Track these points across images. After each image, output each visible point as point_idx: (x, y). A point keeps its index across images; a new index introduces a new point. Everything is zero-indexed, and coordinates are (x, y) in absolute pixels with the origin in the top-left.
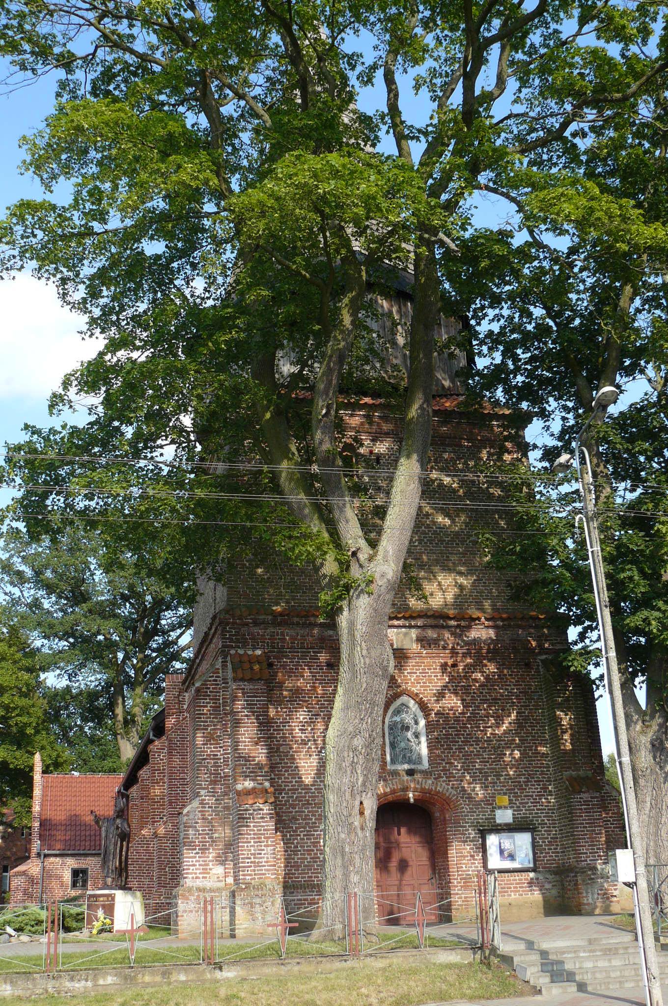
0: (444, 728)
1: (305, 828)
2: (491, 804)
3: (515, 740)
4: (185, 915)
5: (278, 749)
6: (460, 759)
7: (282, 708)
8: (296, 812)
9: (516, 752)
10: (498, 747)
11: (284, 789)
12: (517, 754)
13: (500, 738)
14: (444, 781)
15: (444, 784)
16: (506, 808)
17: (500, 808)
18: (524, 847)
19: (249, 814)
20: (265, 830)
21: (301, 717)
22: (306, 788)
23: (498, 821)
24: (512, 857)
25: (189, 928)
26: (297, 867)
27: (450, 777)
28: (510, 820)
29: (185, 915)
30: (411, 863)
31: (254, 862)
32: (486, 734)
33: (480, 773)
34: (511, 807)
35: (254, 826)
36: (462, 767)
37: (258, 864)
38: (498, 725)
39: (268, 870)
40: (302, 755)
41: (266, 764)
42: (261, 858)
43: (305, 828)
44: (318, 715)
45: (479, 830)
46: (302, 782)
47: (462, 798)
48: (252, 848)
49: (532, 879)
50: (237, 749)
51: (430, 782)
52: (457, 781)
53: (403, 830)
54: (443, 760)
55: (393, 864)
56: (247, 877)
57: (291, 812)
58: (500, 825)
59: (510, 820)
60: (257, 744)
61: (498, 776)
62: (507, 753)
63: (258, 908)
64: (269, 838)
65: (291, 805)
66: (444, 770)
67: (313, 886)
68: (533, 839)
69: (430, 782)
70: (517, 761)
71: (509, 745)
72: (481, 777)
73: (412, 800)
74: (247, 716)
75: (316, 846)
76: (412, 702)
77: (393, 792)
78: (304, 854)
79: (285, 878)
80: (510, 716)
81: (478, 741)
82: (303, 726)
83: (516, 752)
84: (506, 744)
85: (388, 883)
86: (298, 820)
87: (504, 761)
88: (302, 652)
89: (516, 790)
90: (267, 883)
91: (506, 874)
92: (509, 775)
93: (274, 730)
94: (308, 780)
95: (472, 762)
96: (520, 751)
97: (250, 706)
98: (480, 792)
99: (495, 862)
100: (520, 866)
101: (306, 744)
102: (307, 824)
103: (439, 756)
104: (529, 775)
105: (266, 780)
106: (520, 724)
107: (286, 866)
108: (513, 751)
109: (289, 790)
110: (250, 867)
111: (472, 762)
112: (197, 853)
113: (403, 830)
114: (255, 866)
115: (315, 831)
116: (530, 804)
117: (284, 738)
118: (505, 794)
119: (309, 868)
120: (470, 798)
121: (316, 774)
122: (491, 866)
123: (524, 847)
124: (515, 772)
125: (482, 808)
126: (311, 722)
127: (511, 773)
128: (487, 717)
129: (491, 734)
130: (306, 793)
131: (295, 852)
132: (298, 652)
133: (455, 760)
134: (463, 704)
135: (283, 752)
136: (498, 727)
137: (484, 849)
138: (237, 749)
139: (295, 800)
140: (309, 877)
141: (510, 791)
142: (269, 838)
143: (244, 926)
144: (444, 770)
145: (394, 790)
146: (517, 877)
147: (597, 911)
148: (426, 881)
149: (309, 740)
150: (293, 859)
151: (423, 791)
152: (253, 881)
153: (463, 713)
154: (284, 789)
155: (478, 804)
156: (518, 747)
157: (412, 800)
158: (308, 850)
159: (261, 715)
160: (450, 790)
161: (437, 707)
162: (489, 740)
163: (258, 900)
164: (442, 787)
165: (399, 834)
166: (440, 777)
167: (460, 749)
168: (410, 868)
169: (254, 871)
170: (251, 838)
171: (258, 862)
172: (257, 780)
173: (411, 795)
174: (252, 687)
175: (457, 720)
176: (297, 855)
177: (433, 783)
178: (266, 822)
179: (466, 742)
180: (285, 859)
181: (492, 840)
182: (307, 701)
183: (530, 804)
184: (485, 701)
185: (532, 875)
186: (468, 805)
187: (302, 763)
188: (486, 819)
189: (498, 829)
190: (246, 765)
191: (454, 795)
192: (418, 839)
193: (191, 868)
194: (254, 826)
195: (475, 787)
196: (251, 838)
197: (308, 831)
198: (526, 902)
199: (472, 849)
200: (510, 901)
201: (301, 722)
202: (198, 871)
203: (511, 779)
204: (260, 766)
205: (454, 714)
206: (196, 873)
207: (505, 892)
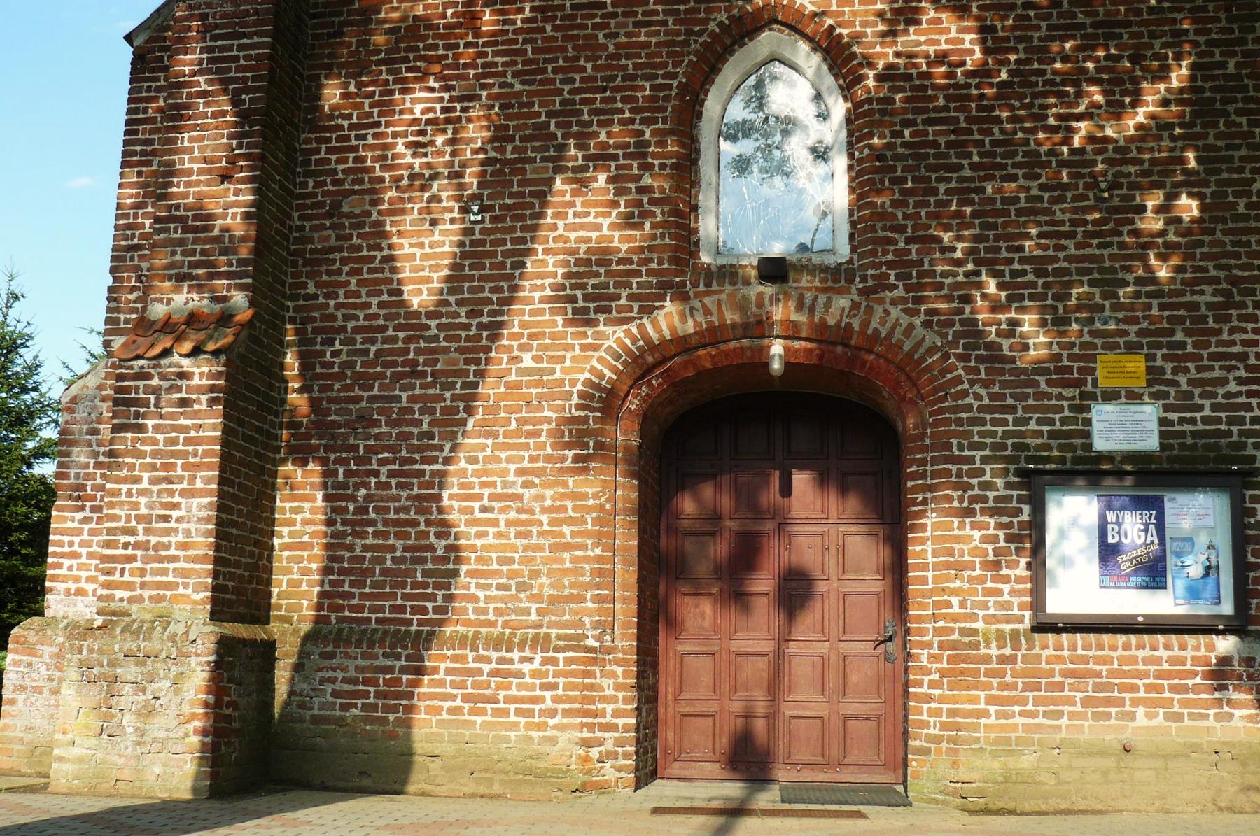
0: (906, 124)
1: (394, 449)
2: (1074, 379)
3: (1183, 161)
4: (20, 698)
5: (337, 205)
6: (965, 225)
7: (360, 85)
8: (372, 399)
9: (1184, 200)
10: (1119, 179)
11: (343, 329)
12: (1189, 207)
13: (1121, 153)
15: (895, 312)
16: (1134, 397)
17: (1111, 396)
18: (1202, 540)
19: (148, 390)
20: (188, 442)
21: (418, 108)
22: (413, 322)
23: (1100, 444)
24: (1154, 572)
25: (29, 737)
26: (359, 574)
27: (921, 287)
28: (1151, 443)
29: (20, 698)
30: (821, 587)
31: (144, 546)
32: (1067, 141)
33: (1039, 273)
34: (1156, 396)
35: (157, 428)
36: (969, 252)
37: (156, 553)
38: (1116, 110)
39: (184, 573)
40: (407, 222)
41: (243, 239)
42: (168, 532)
43: (394, 449)
44: (471, 98)
45: (1020, 473)
46: (403, 304)
47: (964, 358)
48: (143, 500)
49: (1225, 660)
50: (165, 197)
51: (843, 302)
52: (949, 298)
53: (802, 481)
54: (901, 229)
55: (763, 585)
56: (119, 594)
57: (358, 400)
58: (1108, 457)
59: (1151, 443)
60: (225, 177)
61: (1109, 283)
62: (1150, 204)
63: (128, 697)
64: (198, 467)
65: (358, 377)
66: (901, 262)
67: (400, 639)
69: (843, 302)
70: (1188, 232)
71: (1163, 174)
72: (1041, 285)
73: (776, 366)
74: (204, 94)
75: (427, 511)
76: (804, 47)
77: (713, 335)
78: (385, 535)
79: (319, 607)
80: (1166, 78)
81: (1034, 163)
82: (422, 133)
83: (1184, 200)
84: (1145, 174)
85: (735, 646)
86: (377, 424)
87: (1136, 233)
89: (1174, 338)
90: (177, 615)
91: (1121, 639)
92: (1154, 281)
93: (330, 151)
94: (419, 297)
95: (1008, 237)
96: (1200, 196)
97: (217, 65)
98: (1036, 340)
99: (1077, 587)
100: (1182, 610)
101: (423, 188)
103: (883, 216)
104: (1234, 281)
105: (241, 287)
106: (1200, 104)
107: (326, 571)
108: (1171, 197)
109: (357, 330)
110: (131, 559)
111: (1008, 237)
112: (86, 520)
113: (802, 481)
114: (146, 560)
115: (426, 461)
116: (1233, 387)
117: (360, 170)
118: (1132, 348)
119: (397, 577)
120: (994, 358)
121: (448, 279)
122: (1058, 603)
123: (1202, 540)
124: (1178, 269)
125: (1041, 395)
126: (450, 121)
127: (1163, 273)
128: (1076, 84)
129: (1091, 138)
130: (408, 340)
131: (357, 529)
133: (947, 228)
134: (983, 42)
135: (350, 215)
136: (1118, 117)
137: (1032, 539)
138: (165, 197)
139: (372, 364)
140: (395, 609)
141: (1153, 339)
142: (198, 467)
143: (77, 751)
144: (901, 262)
146: (1164, 648)
148: (867, 648)
149: (435, 177)
150: (351, 548)
151: (822, 334)
152: (134, 608)
153: (982, 73)
154: (343, 329)
155: (1024, 379)
156: (1192, 184)
157: (776, 366)
158: (397, 523)
159: (247, 91)
160: (919, 331)
161: (886, 55)
162: (1079, 159)
163: (130, 671)
164: (890, 316)
165: (786, 490)
166: (882, 284)
167: (964, 194)
168: (817, 604)
169: (142, 572)
170: (144, 467)
171: (158, 547)
172: (213, 290)
173: (777, 348)
175: (957, 93)
176: (364, 535)
177: (855, 306)
178: (196, 414)
179: (987, 170)
180: (328, 547)
181: (1072, 515)
182: (439, 59)
184: (1067, 31)
185: (1226, 645)
186: (986, 384)
187: (405, 248)
188: (1053, 435)
189: (1090, 471)
190: (181, 242)
191: (931, 351)
192: (853, 504)
193: (67, 562)
194: (157, 428)
195: (1014, 323)
196: (144, 467)
197: (405, 461)
198: (1196, 748)
199: (994, 539)
200: (1126, 736)
201: (416, 122)
202: (84, 574)
203: (1158, 294)
204: (226, 244)
205: (950, 75)
206: (77, 580)
207: (1109, 702)
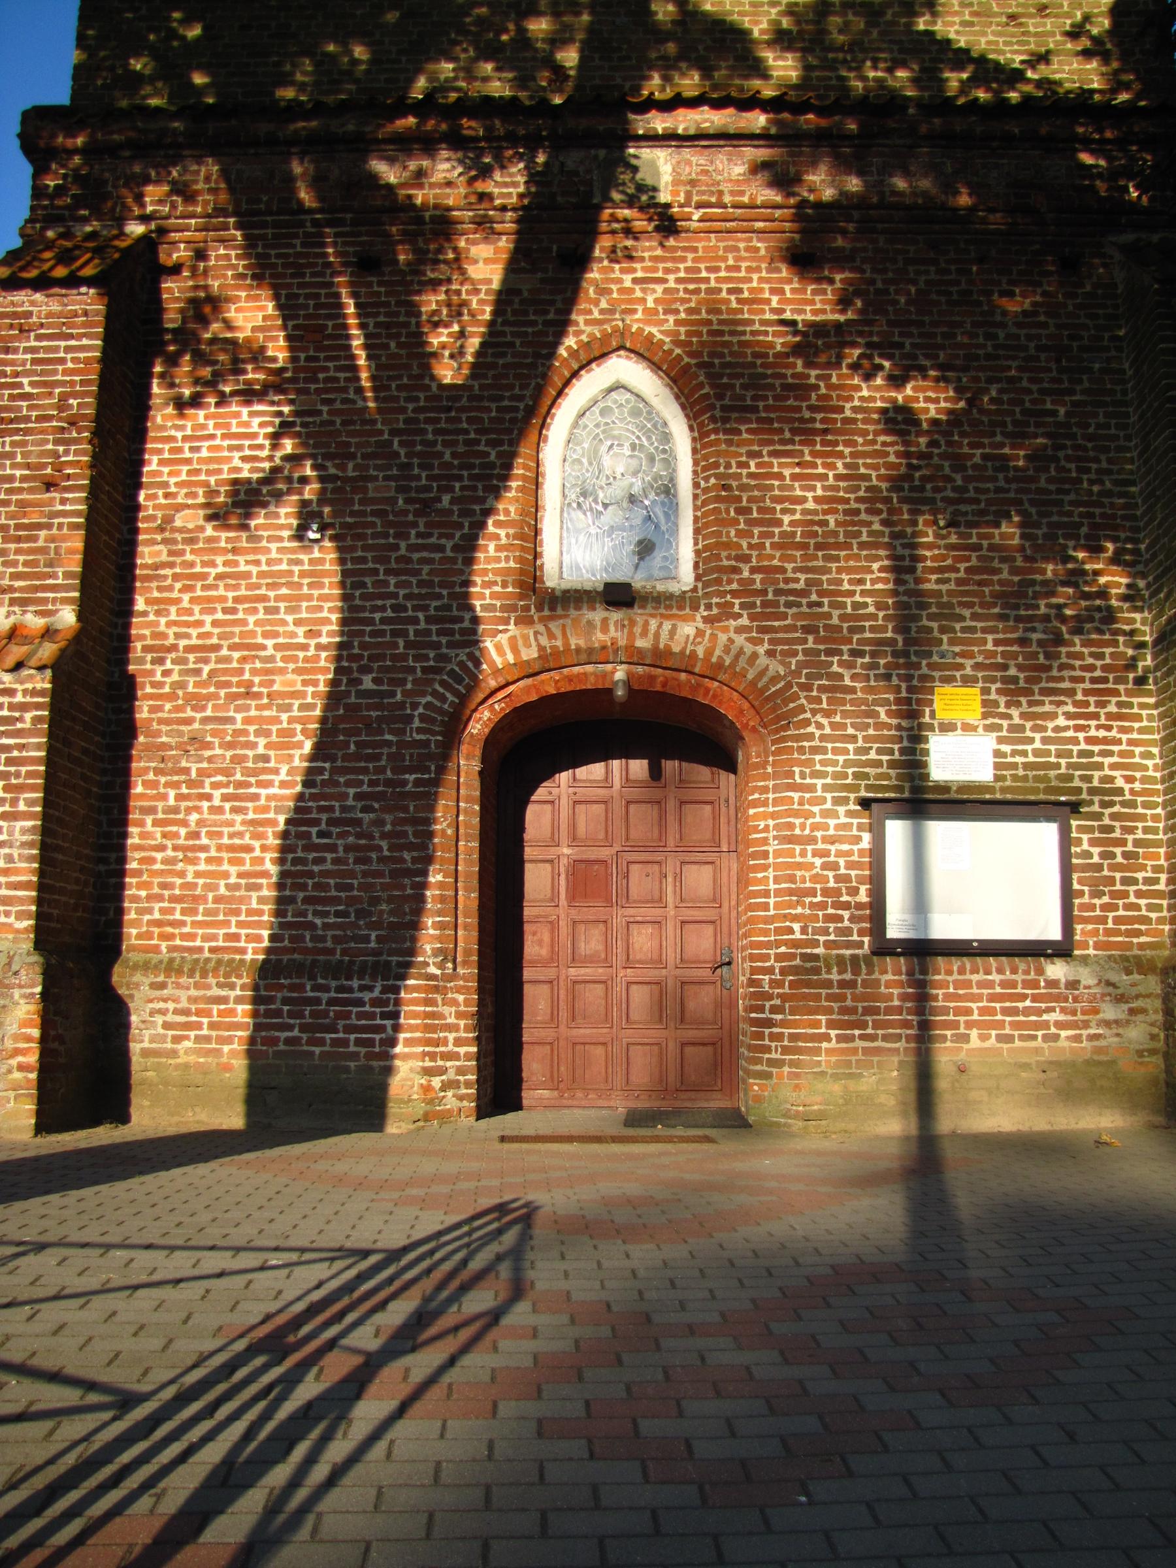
1: (227, 772)
5: (168, 520)
8: (205, 720)
14: (739, 630)
15: (740, 640)
34: (989, 728)
54: (746, 559)
57: (188, 721)
64: (20, 788)
65: (190, 698)
68: (1066, 842)
78: (219, 861)
86: (209, 746)
88: (276, 225)
102: (238, 760)
109: (189, 649)
115: (261, 784)
116: (1061, 721)
130: (243, 660)
132: (264, 225)
135: (181, 530)
142: (20, 788)
145: (556, 653)
147: (573, 911)
150: (182, 874)
158: (231, 848)
159: (75, 395)
160: (763, 661)
174: (55, 307)
177: (700, 633)
178: (19, 733)
183: (1061, 721)
186: (828, 714)
191: (775, 679)
197: (240, 785)
